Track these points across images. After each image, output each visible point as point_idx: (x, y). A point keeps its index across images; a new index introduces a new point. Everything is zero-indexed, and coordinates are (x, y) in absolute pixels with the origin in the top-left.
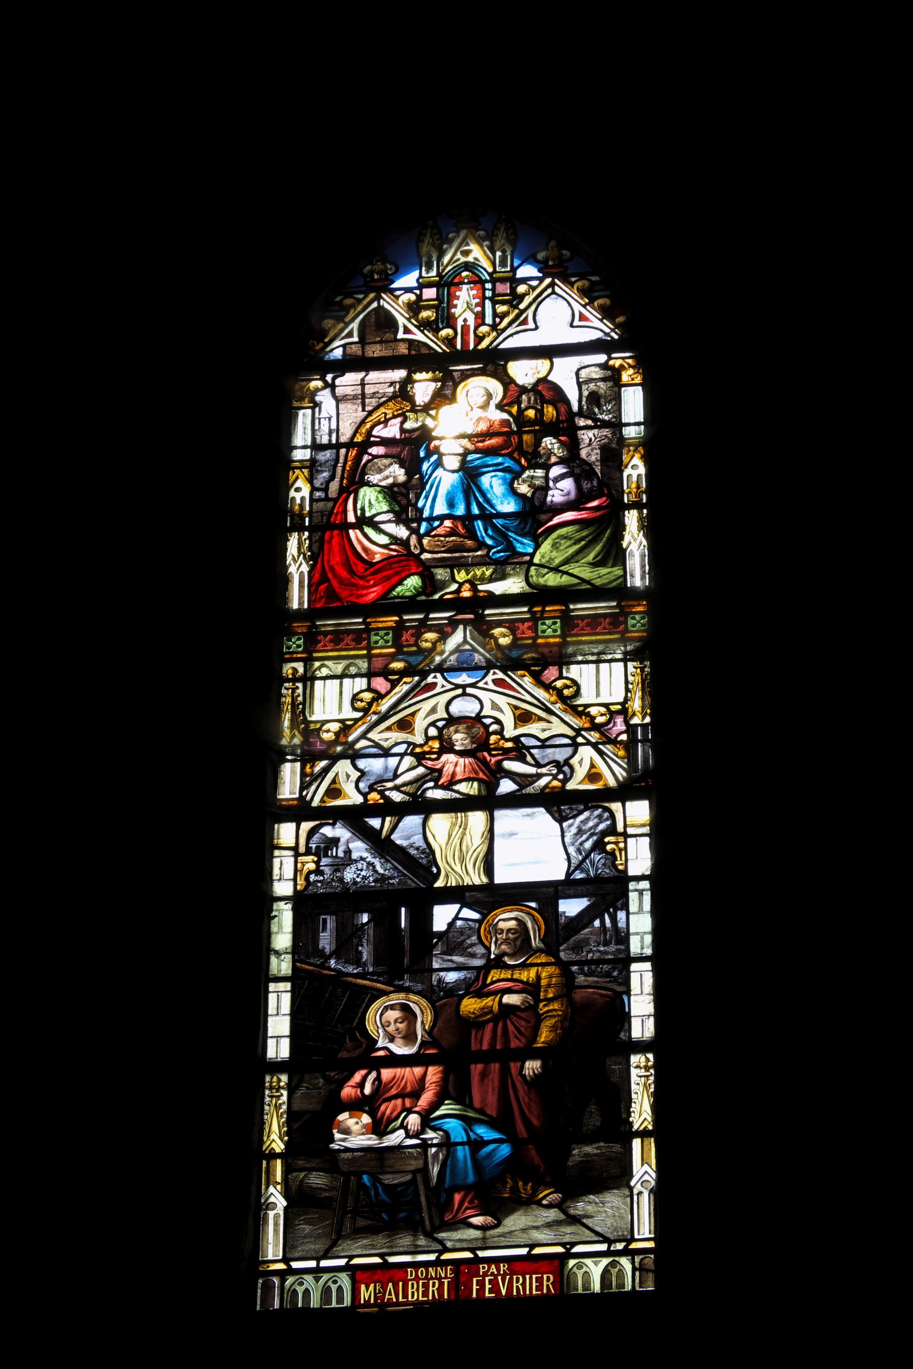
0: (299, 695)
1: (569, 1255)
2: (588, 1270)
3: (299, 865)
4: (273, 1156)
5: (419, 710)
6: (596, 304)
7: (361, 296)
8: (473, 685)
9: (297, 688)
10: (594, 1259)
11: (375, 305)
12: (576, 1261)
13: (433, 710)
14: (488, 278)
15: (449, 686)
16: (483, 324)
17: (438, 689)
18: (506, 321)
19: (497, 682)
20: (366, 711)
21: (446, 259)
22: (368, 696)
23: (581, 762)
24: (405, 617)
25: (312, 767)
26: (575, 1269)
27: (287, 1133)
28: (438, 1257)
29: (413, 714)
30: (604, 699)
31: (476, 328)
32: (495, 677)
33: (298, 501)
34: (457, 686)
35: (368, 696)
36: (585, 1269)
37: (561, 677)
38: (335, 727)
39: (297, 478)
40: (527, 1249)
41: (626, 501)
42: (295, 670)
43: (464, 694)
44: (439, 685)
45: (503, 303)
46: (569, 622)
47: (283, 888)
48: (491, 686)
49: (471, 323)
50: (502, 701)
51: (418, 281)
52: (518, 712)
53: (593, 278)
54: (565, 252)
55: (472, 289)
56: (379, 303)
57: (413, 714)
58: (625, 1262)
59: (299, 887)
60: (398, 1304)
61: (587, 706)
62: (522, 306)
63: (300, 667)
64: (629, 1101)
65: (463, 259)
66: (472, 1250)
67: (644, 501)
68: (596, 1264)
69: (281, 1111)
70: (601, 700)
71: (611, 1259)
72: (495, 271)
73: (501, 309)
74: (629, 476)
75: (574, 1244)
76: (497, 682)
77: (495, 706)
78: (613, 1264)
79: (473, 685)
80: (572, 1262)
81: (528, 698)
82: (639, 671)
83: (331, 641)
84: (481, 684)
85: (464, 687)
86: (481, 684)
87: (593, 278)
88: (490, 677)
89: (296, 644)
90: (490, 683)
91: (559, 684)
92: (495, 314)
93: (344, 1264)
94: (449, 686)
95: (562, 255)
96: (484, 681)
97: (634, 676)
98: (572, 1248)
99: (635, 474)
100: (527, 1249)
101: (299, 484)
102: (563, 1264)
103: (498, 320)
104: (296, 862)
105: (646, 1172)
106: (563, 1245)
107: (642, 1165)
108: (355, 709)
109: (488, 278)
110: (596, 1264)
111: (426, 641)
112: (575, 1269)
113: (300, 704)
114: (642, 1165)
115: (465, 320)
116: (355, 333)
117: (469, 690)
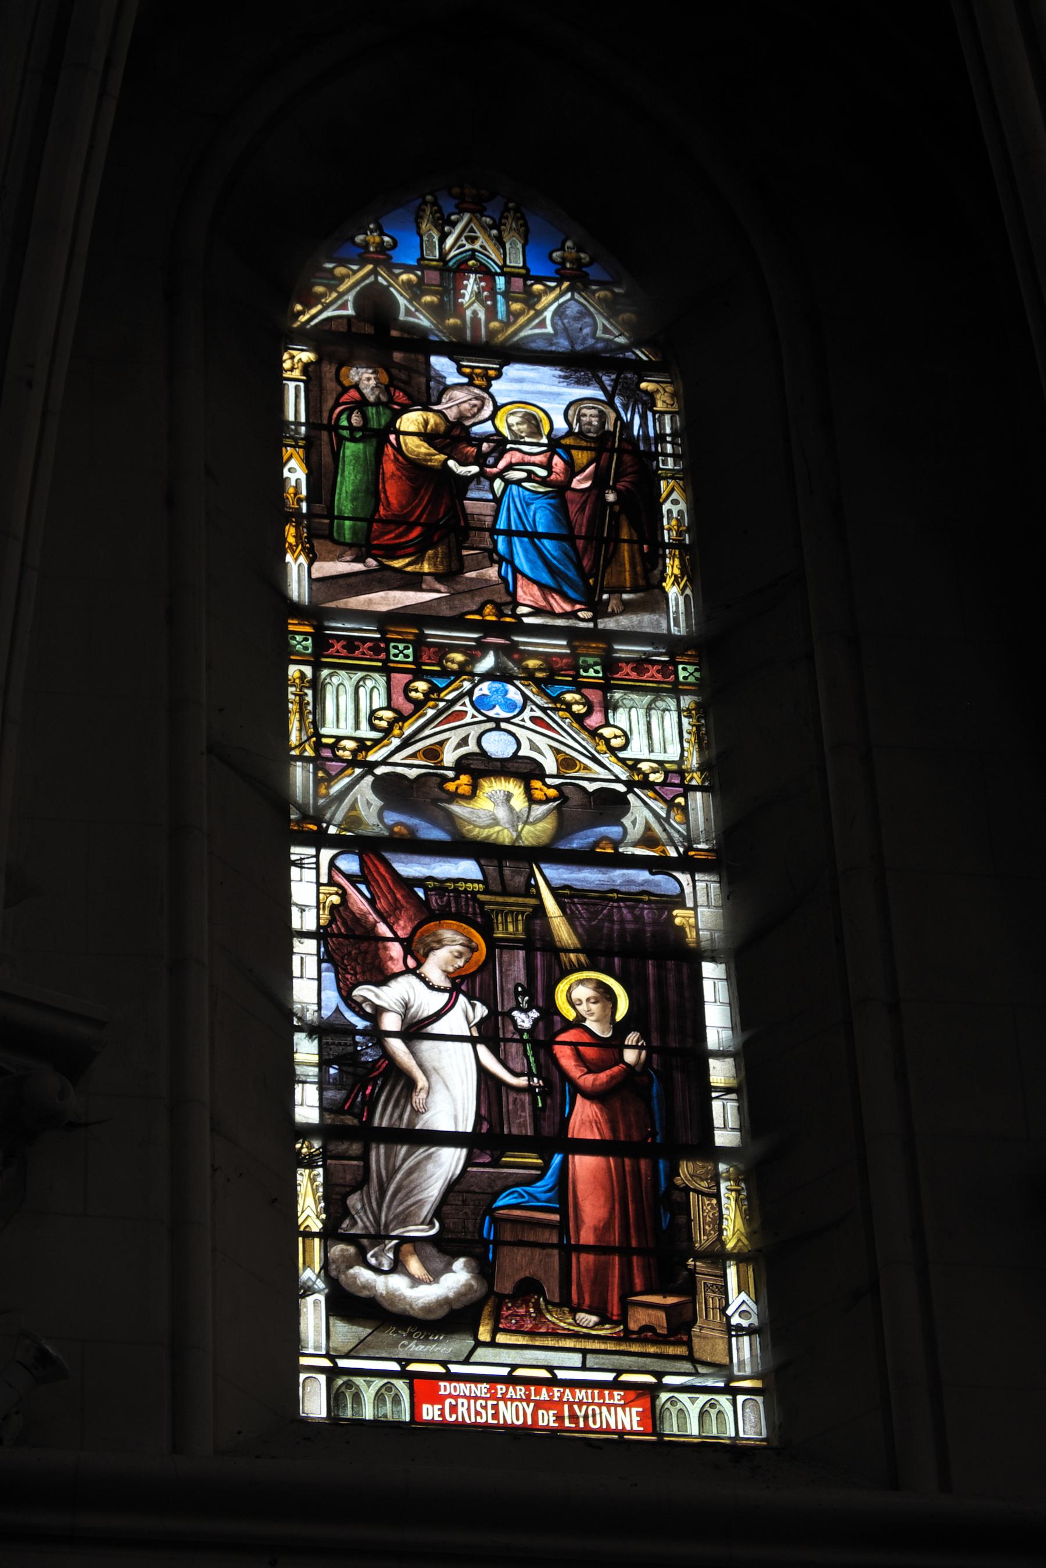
0: (308, 703)
1: (660, 1387)
2: (682, 1407)
3: (321, 896)
4: (308, 1235)
5: (448, 739)
6: (620, 318)
7: (355, 267)
8: (507, 720)
9: (306, 694)
10: (368, 1379)
11: (372, 279)
12: (345, 1378)
13: (464, 742)
14: (498, 271)
15: (481, 718)
16: (495, 319)
17: (468, 719)
18: (522, 320)
19: (533, 719)
20: (387, 732)
21: (449, 242)
22: (389, 714)
23: (634, 823)
24: (427, 632)
25: (328, 788)
26: (343, 1389)
27: (326, 1210)
28: (616, 1378)
29: (441, 743)
30: (658, 756)
31: (487, 322)
32: (533, 714)
33: (293, 483)
34: (490, 719)
35: (389, 714)
36: (679, 1406)
37: (607, 724)
38: (351, 745)
39: (291, 457)
40: (614, 1374)
41: (666, 540)
42: (303, 675)
43: (498, 728)
44: (469, 715)
45: (516, 300)
46: (610, 665)
47: (304, 920)
48: (529, 724)
49: (482, 315)
50: (542, 742)
51: (418, 261)
52: (561, 757)
53: (617, 290)
54: (583, 255)
55: (481, 280)
56: (376, 278)
57: (441, 743)
58: (724, 1400)
59: (322, 922)
60: (569, 1430)
61: (638, 761)
62: (342, 288)
63: (308, 671)
64: (295, 1195)
65: (468, 246)
66: (444, 1363)
67: (687, 542)
68: (693, 1401)
69: (317, 1183)
70: (653, 757)
71: (386, 1381)
72: (505, 265)
73: (516, 306)
74: (670, 511)
75: (409, 1361)
76: (533, 719)
77: (534, 747)
78: (388, 1387)
79: (507, 720)
80: (664, 1396)
81: (427, 732)
82: (694, 729)
83: (370, 649)
84: (516, 720)
85: (497, 721)
86: (516, 720)
87: (617, 290)
88: (527, 714)
89: (303, 644)
90: (527, 719)
91: (607, 732)
92: (509, 312)
93: (506, 1374)
94: (481, 718)
95: (382, 241)
96: (520, 718)
97: (690, 733)
98: (407, 1364)
99: (675, 510)
100: (614, 1374)
101: (293, 463)
102: (654, 1398)
103: (512, 319)
104: (318, 893)
105: (744, 1302)
106: (399, 1361)
107: (739, 1293)
108: (373, 727)
109: (498, 271)
110: (693, 1401)
111: (453, 662)
112: (668, 1405)
113: (309, 712)
114: (739, 1293)
115: (475, 313)
116: (350, 305)
117: (503, 725)
